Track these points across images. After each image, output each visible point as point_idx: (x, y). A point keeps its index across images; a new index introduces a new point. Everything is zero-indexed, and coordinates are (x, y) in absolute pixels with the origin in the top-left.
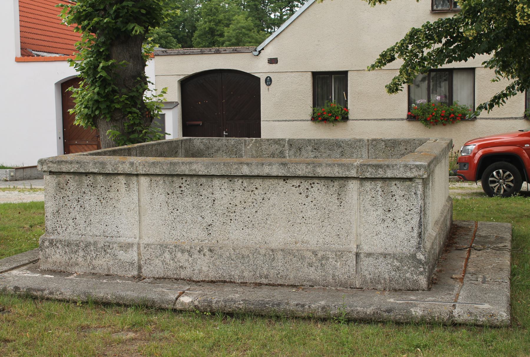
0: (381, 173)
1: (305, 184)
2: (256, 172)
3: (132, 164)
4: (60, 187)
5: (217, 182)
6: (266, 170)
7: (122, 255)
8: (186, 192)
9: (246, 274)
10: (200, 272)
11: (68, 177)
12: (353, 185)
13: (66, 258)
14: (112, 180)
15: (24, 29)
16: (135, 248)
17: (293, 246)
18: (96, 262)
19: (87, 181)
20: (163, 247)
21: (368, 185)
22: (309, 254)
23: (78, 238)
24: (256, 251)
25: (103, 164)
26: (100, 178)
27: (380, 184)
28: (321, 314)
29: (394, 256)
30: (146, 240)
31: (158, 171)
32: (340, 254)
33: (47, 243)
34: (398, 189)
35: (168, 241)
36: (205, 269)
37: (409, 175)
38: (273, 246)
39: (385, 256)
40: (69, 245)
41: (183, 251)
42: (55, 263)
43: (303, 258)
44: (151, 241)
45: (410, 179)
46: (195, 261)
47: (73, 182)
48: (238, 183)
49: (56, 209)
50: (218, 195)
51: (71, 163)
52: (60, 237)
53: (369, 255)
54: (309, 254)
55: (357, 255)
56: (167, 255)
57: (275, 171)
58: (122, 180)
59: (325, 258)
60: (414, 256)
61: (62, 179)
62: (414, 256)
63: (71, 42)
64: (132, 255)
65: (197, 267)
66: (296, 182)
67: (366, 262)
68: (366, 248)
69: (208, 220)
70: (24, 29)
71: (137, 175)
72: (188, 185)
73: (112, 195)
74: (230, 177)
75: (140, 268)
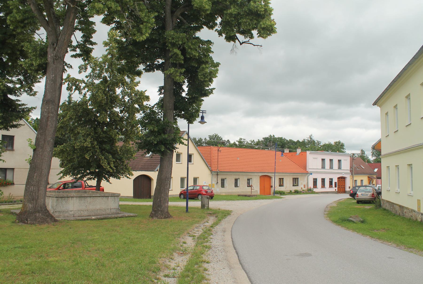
0: (114, 195)
1: (102, 197)
2: (96, 196)
3: (73, 195)
4: (57, 200)
5: (88, 198)
6: (97, 195)
7: (71, 213)
8: (83, 200)
9: (93, 214)
10: (85, 214)
11: (59, 198)
12: (110, 197)
13: (59, 214)
14: (68, 198)
15: (306, 160)
16: (73, 211)
17: (100, 208)
18: (65, 215)
19: (63, 198)
20: (78, 210)
21: (112, 197)
22: (103, 209)
23: (61, 210)
24: (95, 210)
25: (68, 195)
26: (66, 198)
27: (113, 197)
28: (114, 217)
29: (116, 209)
30: (75, 210)
31: (78, 196)
32: (108, 209)
33: (55, 212)
34: (116, 198)
35: (79, 209)
36: (86, 214)
37: (118, 195)
38: (98, 209)
39: (115, 209)
40: (59, 211)
41: (82, 211)
42: (56, 216)
43: (102, 210)
44: (76, 210)
45: (118, 196)
46: (84, 213)
47: (60, 199)
48: (92, 198)
49: (56, 205)
50: (88, 200)
51: (61, 195)
52: (57, 210)
53: (112, 209)
54: (103, 209)
55: (111, 209)
56: (79, 212)
57: (99, 195)
58: (71, 198)
59: (106, 210)
60: (118, 208)
61: (58, 198)
62: (118, 208)
63: (279, 161)
64: (73, 213)
65: (84, 214)
66: (101, 197)
67: (112, 210)
68: (112, 208)
69: (86, 205)
70: (306, 160)
71: (73, 197)
72: (83, 199)
73: (68, 201)
74: (90, 197)
75: (74, 215)
